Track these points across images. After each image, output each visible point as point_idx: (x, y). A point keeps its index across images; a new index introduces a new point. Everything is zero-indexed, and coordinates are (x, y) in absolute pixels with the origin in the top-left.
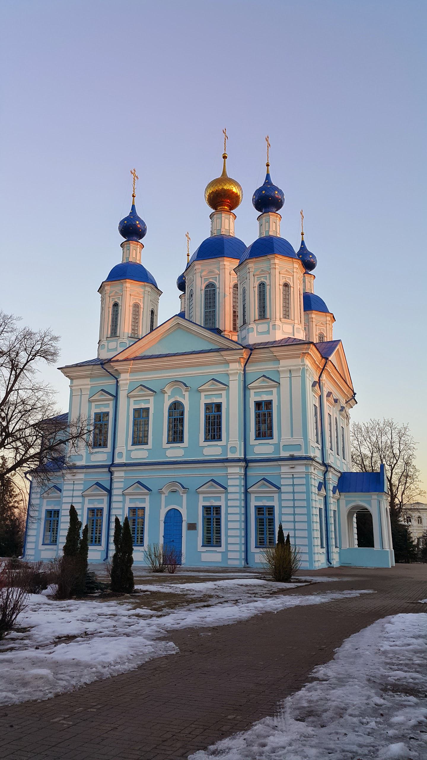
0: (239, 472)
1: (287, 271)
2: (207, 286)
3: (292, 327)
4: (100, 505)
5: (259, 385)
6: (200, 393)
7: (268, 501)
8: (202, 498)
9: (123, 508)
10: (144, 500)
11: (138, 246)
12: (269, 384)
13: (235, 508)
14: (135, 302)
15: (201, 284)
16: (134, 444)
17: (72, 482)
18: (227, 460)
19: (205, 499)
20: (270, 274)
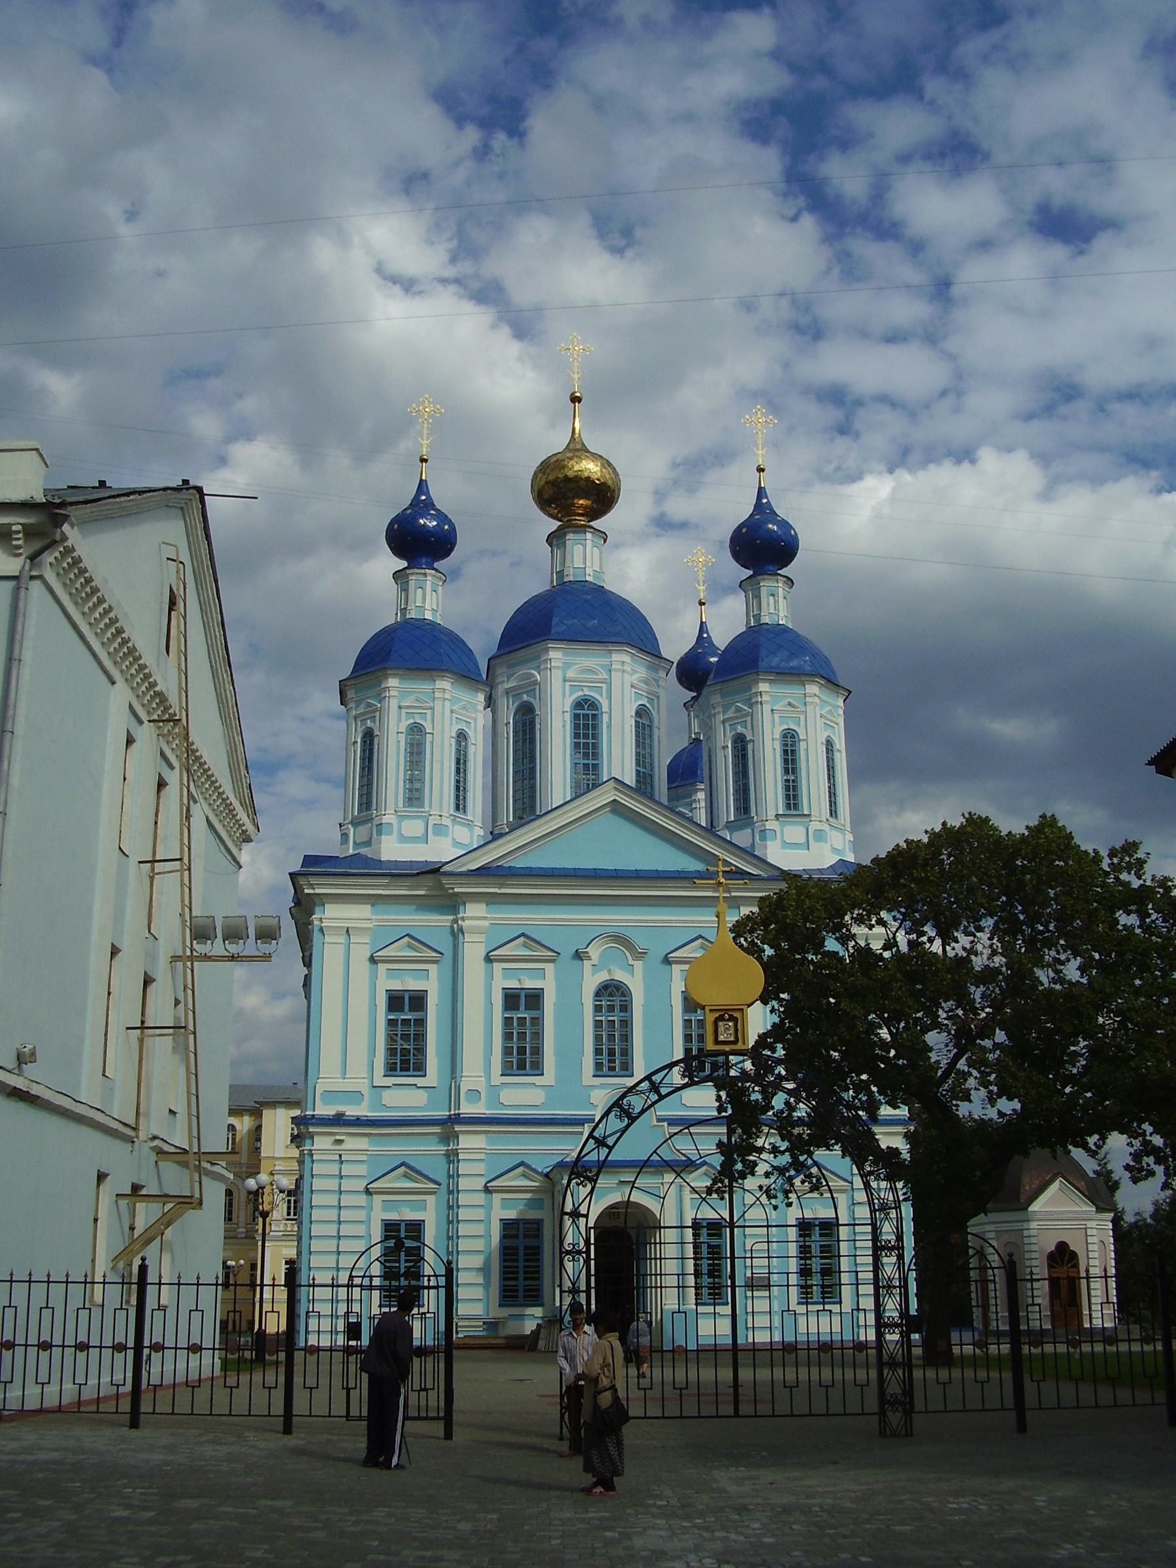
0: (483, 1146)
1: (790, 704)
2: (579, 705)
3: (804, 830)
4: (415, 1213)
5: (690, 955)
6: (580, 962)
7: (414, 1210)
8: (380, 1204)
9: (368, 1222)
11: (780, 585)
12: (421, 955)
13: (326, 1226)
14: (786, 727)
15: (564, 697)
16: (391, 1069)
17: (337, 1157)
20: (432, 708)
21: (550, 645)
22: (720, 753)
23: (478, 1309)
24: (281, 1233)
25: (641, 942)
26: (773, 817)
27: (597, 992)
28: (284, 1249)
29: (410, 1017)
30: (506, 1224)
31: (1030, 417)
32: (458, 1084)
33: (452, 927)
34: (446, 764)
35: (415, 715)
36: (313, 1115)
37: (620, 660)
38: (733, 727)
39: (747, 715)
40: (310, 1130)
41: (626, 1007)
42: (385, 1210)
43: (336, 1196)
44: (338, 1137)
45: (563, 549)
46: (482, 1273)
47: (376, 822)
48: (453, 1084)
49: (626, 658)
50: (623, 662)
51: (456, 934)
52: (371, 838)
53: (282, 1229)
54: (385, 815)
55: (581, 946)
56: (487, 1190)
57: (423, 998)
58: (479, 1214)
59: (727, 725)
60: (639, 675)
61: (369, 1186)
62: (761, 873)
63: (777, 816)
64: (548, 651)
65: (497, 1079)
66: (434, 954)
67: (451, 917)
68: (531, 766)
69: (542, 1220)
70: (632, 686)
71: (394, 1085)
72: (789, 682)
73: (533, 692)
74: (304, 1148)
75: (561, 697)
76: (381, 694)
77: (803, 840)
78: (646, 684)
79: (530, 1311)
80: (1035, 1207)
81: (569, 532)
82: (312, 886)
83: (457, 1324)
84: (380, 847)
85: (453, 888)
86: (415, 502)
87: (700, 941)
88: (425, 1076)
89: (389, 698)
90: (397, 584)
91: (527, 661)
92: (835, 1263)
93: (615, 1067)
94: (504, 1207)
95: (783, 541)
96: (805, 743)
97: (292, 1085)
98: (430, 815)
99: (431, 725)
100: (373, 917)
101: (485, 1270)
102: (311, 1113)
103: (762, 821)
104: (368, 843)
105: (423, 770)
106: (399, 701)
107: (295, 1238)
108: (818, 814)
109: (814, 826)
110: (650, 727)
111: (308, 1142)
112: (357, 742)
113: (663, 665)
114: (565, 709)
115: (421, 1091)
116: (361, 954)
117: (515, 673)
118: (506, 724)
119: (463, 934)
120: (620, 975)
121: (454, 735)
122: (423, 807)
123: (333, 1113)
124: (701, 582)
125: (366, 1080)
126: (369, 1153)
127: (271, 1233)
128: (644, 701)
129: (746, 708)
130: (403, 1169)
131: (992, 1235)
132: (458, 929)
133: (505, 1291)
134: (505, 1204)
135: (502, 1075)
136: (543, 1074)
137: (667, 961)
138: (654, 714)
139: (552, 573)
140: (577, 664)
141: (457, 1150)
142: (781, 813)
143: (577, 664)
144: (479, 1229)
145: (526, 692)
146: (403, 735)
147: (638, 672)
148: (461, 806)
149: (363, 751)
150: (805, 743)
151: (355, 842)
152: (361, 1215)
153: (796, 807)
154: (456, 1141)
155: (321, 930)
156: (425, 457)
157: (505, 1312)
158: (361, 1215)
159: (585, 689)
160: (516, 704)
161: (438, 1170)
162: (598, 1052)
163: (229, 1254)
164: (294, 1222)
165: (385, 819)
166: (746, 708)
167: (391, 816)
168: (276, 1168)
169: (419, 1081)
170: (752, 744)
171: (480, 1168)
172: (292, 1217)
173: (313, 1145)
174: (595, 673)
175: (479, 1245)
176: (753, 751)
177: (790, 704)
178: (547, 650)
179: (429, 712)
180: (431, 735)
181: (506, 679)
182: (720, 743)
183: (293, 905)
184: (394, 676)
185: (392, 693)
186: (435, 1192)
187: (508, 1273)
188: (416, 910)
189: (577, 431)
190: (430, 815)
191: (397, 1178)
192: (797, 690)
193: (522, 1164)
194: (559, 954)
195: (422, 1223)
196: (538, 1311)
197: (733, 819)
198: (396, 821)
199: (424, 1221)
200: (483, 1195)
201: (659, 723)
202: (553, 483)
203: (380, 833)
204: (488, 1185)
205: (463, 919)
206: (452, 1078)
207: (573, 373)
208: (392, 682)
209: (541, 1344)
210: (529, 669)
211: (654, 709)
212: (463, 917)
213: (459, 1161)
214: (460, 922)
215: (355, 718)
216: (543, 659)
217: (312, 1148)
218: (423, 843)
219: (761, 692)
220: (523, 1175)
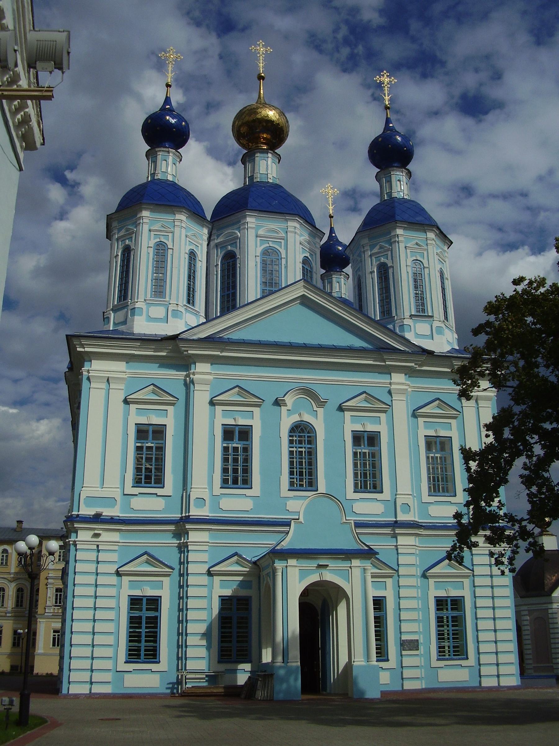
0: (207, 540)
1: (417, 244)
3: (429, 327)
5: (357, 405)
8: (128, 583)
10: (160, 586)
15: (256, 247)
16: (137, 482)
17: (95, 547)
18: (396, 524)
19: (132, 584)
20: (173, 233)
21: (247, 213)
22: (369, 276)
23: (202, 665)
24: (51, 614)
25: (323, 394)
26: (408, 317)
27: (290, 431)
28: (53, 623)
29: (152, 445)
30: (224, 600)
31: (449, 205)
32: (188, 494)
33: (185, 380)
34: (182, 270)
35: (161, 236)
36: (78, 515)
37: (294, 225)
38: (378, 258)
39: (388, 250)
40: (75, 526)
41: (312, 440)
42: (131, 588)
43: (94, 577)
44: (96, 532)
45: (253, 163)
46: (205, 637)
47: (130, 307)
48: (184, 494)
49: (297, 225)
50: (295, 227)
51: (188, 385)
52: (126, 319)
53: (52, 611)
54: (137, 302)
55: (280, 395)
56: (210, 573)
57: (163, 431)
58: (203, 592)
59: (373, 258)
60: (304, 238)
61: (119, 570)
62: (407, 349)
63: (411, 316)
64: (246, 217)
65: (218, 491)
66: (172, 399)
67: (185, 373)
68: (233, 291)
69: (251, 597)
70: (300, 243)
71: (139, 493)
72: (417, 230)
73: (235, 244)
74: (70, 540)
75: (254, 247)
76: (136, 222)
77: (429, 333)
78: (308, 244)
79: (241, 666)
80: (555, 594)
81: (257, 152)
82: (83, 346)
83: (185, 676)
84: (133, 324)
85: (187, 351)
86: (163, 109)
87: (364, 395)
88: (163, 487)
89: (142, 224)
90: (148, 159)
91: (234, 224)
92: (384, 630)
93: (303, 484)
94: (222, 587)
95: (405, 147)
96: (428, 269)
97: (60, 529)
98: (170, 304)
99: (172, 244)
100: (127, 371)
101: (207, 635)
102: (77, 513)
103: (401, 319)
104: (125, 323)
105: (165, 273)
106: (149, 227)
107: (61, 617)
108: (438, 317)
109: (436, 324)
110: (311, 272)
111: (73, 535)
112: (118, 255)
113: (318, 234)
114: (257, 255)
115: (160, 499)
116: (118, 396)
117: (222, 233)
118: (216, 266)
119: (194, 385)
120: (307, 418)
121: (187, 252)
122: (165, 298)
123: (93, 513)
124: (331, 204)
125: (118, 490)
126: (119, 544)
127: (46, 614)
128: (308, 255)
129: (387, 246)
130: (145, 557)
131: (526, 613)
132: (190, 382)
133: (222, 651)
134: (223, 584)
135: (221, 488)
136: (251, 488)
137: (341, 409)
138: (314, 264)
139: (245, 178)
140: (265, 226)
141: (187, 542)
142: (413, 314)
143: (265, 226)
144: (203, 603)
145: (230, 245)
146: (152, 249)
147: (304, 236)
148: (191, 301)
149: (123, 261)
150: (428, 269)
151: (114, 323)
152: (113, 592)
153: (423, 311)
154: (186, 536)
155: (88, 379)
156: (170, 84)
157: (222, 667)
158: (113, 592)
159: (270, 242)
160: (223, 252)
161: (172, 558)
162: (291, 473)
163: (19, 626)
164: (59, 607)
165: (137, 305)
166: (387, 246)
167: (142, 303)
168: (50, 575)
169: (159, 491)
170: (392, 269)
171: (205, 557)
172: (58, 604)
173: (77, 538)
174: (277, 233)
175: (203, 615)
176: (393, 273)
177: (417, 244)
178: (245, 217)
179: (170, 235)
180: (171, 250)
181: (216, 238)
182: (369, 269)
183: (67, 370)
184: (146, 209)
185: (144, 221)
186: (170, 575)
187: (224, 637)
188: (159, 367)
189: (262, 96)
190: (170, 304)
191: (140, 564)
192: (422, 235)
193: (236, 554)
194: (264, 400)
195: (159, 598)
196: (247, 667)
197: (379, 319)
198: (145, 306)
199: (161, 597)
200: (206, 577)
201: (316, 270)
202: (247, 124)
203: (133, 314)
204: (211, 570)
205: (194, 374)
206: (184, 490)
207: (260, 63)
208: (145, 213)
209: (259, 694)
210: (233, 230)
211: (313, 260)
212: (194, 372)
213: (188, 551)
214: (191, 376)
215: (118, 240)
216: (243, 222)
217: (76, 540)
218: (165, 323)
219: (398, 235)
220: (237, 563)
